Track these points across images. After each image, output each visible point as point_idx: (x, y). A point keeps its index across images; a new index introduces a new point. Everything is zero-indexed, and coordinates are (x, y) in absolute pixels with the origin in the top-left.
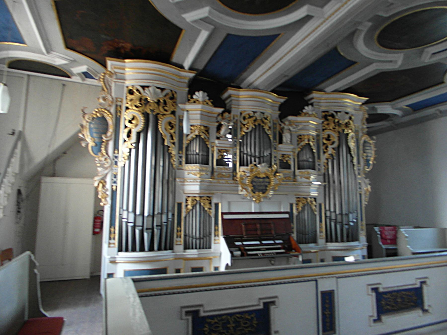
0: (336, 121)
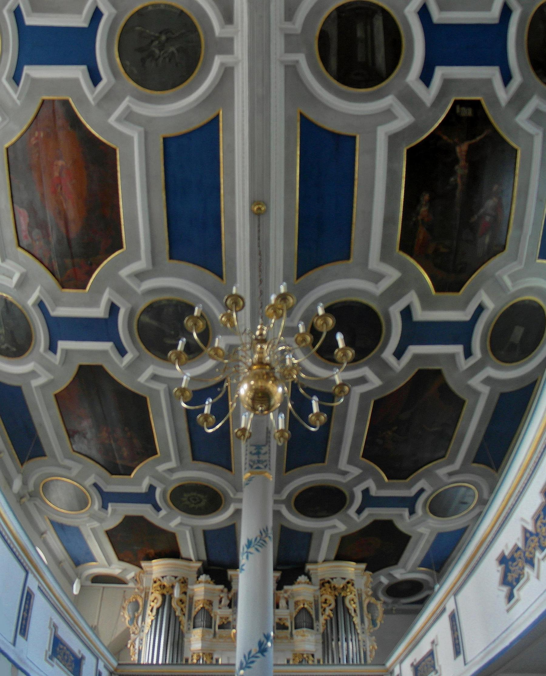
0: (332, 586)
